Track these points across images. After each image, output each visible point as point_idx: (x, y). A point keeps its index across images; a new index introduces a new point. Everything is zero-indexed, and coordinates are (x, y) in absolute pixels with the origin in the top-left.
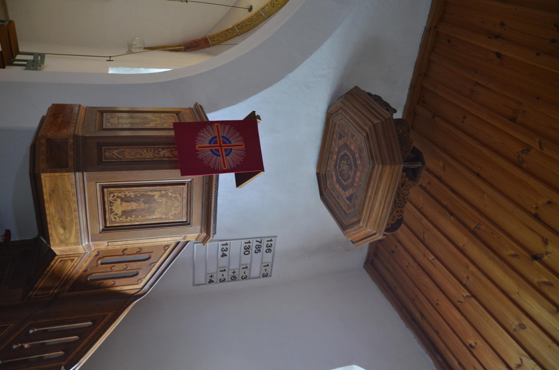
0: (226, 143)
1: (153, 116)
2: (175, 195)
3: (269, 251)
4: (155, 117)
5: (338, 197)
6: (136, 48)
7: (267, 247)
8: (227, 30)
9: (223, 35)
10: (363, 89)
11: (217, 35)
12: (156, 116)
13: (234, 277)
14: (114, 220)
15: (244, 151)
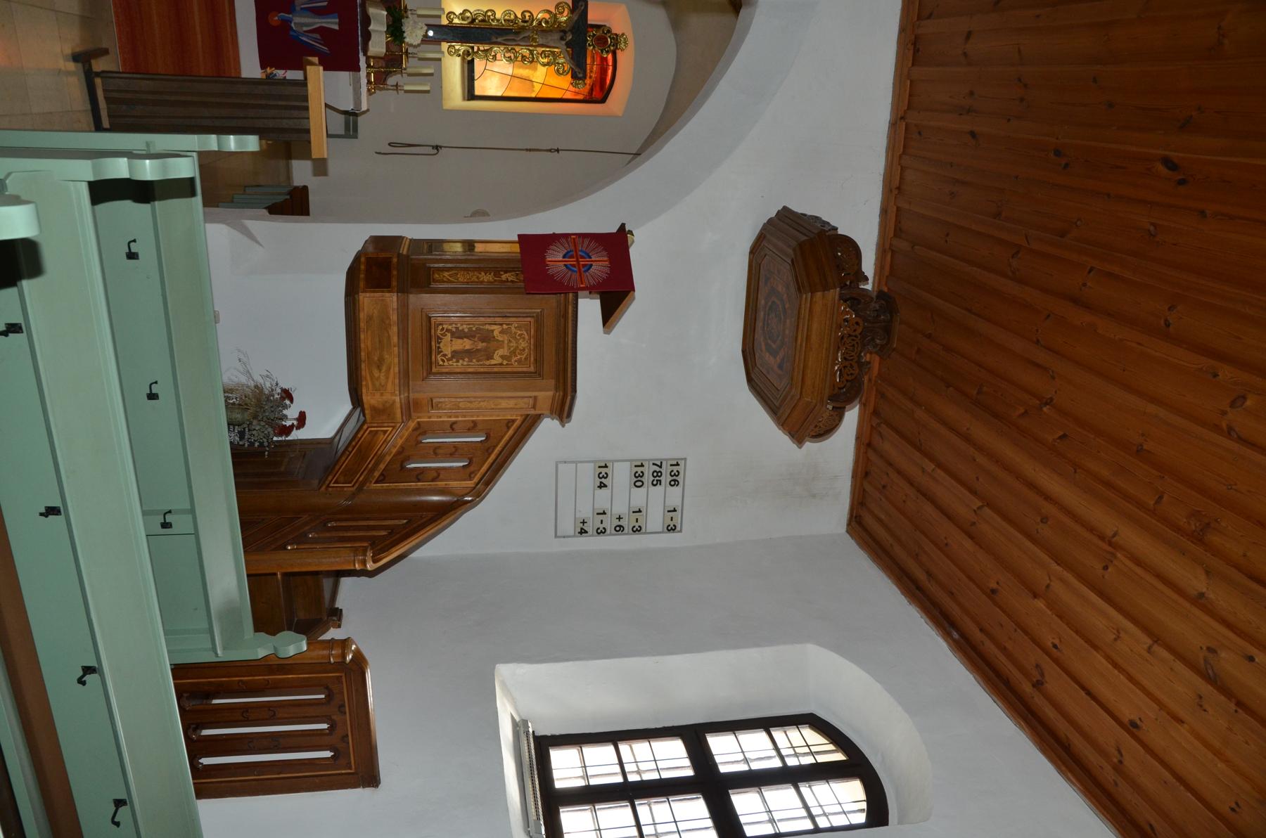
0: (584, 258)
2: (520, 331)
3: (675, 483)
5: (768, 373)
7: (672, 476)
10: (800, 211)
13: (620, 526)
14: (441, 363)
15: (610, 267)
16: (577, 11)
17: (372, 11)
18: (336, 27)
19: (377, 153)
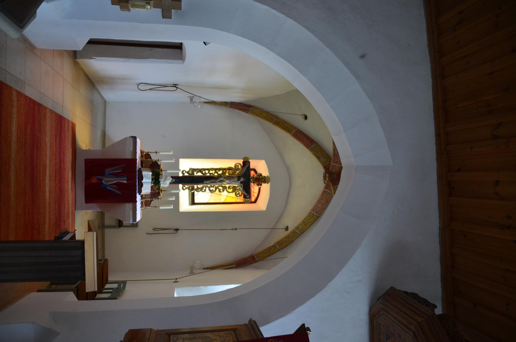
1: (214, 335)
4: (215, 336)
6: (197, 269)
8: (270, 248)
9: (267, 251)
11: (262, 252)
12: (216, 334)
16: (245, 167)
17: (144, 173)
18: (126, 182)
19: (147, 233)
